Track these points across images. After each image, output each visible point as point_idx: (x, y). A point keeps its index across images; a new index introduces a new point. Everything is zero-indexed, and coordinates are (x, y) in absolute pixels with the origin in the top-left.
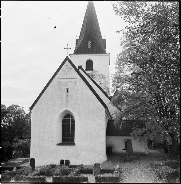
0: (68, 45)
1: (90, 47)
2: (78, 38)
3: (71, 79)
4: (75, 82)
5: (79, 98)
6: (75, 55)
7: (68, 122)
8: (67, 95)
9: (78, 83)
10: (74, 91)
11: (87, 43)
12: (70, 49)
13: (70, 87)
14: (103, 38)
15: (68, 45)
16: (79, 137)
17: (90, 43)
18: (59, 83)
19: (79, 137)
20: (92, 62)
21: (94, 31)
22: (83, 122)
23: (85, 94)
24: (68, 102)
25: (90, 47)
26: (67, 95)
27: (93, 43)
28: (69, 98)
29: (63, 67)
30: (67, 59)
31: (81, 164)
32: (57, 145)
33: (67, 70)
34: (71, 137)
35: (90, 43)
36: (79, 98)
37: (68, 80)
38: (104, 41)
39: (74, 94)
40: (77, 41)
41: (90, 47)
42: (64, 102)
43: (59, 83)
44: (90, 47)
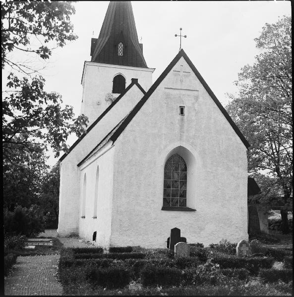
0: (181, 29)
1: (120, 53)
2: (97, 37)
3: (189, 91)
4: (197, 98)
5: (203, 126)
6: (96, 64)
7: (177, 167)
8: (182, 120)
9: (201, 99)
10: (194, 113)
11: (116, 46)
12: (176, 36)
13: (187, 105)
14: (140, 43)
15: (181, 29)
16: (202, 197)
17: (121, 46)
18: (168, 97)
19: (202, 197)
20: (125, 80)
21: (128, 28)
22: (210, 171)
23: (212, 121)
24: (183, 132)
25: (120, 54)
26: (182, 120)
27: (125, 48)
28: (186, 125)
29: (174, 68)
30: (182, 54)
31: (138, 245)
32: (194, 210)
33: (181, 73)
34: (173, 196)
35: (121, 46)
36: (203, 126)
37: (183, 92)
38: (141, 45)
39: (193, 118)
40: (94, 41)
41: (120, 54)
42: (177, 131)
43: (168, 97)
44: (120, 53)
